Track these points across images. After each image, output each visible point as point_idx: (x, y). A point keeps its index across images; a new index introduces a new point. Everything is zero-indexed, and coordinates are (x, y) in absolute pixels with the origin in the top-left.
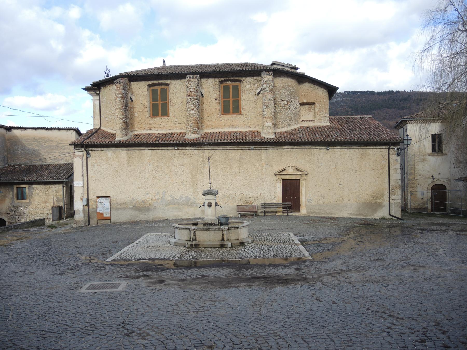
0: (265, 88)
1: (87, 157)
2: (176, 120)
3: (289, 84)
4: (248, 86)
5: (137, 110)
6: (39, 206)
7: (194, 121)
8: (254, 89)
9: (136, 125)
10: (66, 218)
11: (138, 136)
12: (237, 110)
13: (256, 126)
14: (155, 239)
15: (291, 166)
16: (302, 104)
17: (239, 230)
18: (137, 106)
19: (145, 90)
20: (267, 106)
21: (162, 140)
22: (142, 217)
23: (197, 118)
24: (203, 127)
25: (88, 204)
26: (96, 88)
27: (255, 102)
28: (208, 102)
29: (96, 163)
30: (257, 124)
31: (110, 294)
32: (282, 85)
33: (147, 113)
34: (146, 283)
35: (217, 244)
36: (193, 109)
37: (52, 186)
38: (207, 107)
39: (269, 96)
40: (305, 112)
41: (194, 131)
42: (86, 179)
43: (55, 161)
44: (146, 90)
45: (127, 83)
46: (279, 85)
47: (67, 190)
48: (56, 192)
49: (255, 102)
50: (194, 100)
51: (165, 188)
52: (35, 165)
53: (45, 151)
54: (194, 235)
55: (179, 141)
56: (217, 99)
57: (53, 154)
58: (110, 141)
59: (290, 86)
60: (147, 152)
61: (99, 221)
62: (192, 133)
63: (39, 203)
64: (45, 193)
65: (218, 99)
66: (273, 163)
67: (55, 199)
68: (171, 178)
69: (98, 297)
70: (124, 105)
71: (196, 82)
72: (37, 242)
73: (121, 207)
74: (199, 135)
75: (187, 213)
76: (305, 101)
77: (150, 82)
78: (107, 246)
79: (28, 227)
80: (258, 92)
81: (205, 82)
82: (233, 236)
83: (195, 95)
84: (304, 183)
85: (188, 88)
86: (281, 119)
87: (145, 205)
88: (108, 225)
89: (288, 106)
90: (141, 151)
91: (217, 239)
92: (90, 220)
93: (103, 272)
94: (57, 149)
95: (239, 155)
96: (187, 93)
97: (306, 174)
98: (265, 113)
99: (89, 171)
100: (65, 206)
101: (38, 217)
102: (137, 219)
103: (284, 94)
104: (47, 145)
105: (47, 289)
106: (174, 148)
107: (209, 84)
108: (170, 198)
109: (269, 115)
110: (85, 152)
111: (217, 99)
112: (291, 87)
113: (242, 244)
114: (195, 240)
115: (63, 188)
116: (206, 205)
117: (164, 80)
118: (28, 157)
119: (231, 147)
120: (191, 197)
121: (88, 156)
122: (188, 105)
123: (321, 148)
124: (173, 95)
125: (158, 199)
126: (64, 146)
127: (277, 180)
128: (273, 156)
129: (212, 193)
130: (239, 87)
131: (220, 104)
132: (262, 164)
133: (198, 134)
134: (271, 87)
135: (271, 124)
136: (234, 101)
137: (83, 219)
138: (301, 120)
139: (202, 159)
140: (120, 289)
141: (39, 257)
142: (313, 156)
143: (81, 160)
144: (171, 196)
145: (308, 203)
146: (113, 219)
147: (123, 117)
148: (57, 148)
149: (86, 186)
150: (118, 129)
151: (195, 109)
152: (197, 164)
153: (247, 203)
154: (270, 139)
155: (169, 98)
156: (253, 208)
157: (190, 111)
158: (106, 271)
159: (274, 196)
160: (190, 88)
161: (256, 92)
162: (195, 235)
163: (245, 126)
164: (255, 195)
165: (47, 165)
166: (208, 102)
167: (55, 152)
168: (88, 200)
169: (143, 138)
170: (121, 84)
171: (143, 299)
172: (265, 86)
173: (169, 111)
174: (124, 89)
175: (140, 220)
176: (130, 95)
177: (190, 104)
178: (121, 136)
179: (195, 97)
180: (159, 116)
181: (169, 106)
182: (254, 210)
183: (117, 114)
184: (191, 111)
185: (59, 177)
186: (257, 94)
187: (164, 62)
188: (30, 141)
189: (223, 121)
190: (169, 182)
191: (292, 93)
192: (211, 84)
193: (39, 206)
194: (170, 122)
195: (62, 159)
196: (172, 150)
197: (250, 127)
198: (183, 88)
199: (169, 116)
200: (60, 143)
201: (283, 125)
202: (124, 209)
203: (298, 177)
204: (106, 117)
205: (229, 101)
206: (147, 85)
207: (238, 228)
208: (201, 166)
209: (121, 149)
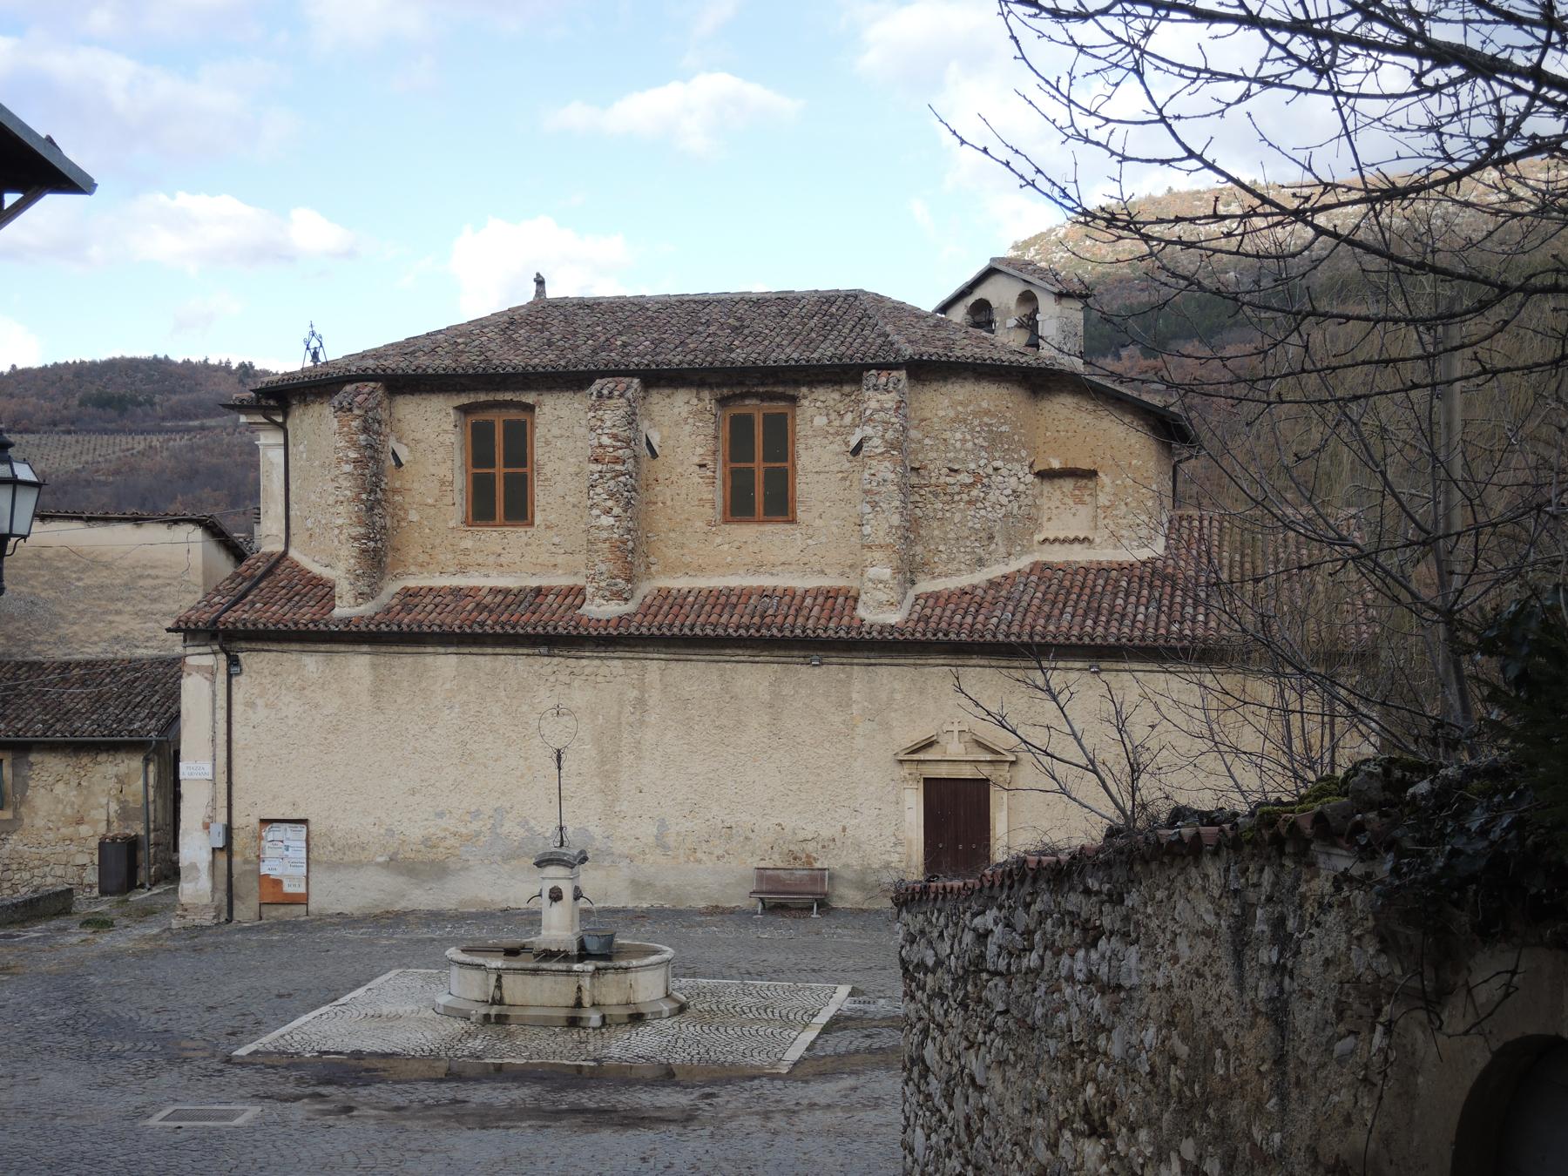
0: (870, 438)
1: (230, 676)
2: (556, 540)
3: (985, 405)
4: (820, 421)
6: (51, 836)
7: (612, 552)
9: (414, 552)
10: (154, 884)
11: (417, 600)
12: (780, 505)
13: (847, 570)
14: (405, 991)
15: (956, 728)
16: (1046, 475)
17: (631, 976)
18: (416, 485)
20: (874, 505)
21: (496, 623)
22: (421, 898)
23: (624, 543)
24: (653, 568)
25: (228, 847)
26: (272, 403)
27: (844, 479)
28: (674, 478)
29: (261, 696)
30: (849, 562)
31: (211, 1130)
32: (952, 414)
34: (309, 1111)
36: (608, 511)
37: (102, 757)
38: (668, 493)
39: (882, 468)
40: (1058, 504)
41: (611, 591)
42: (225, 754)
43: (117, 647)
44: (451, 427)
45: (379, 404)
46: (941, 413)
47: (159, 774)
48: (121, 780)
49: (844, 479)
50: (613, 478)
51: (503, 793)
52: (39, 665)
53: (81, 606)
55: (555, 628)
56: (704, 466)
57: (110, 618)
58: (312, 621)
59: (987, 412)
60: (445, 664)
61: (264, 908)
62: (603, 597)
63: (51, 825)
64: (74, 783)
65: (711, 465)
66: (893, 714)
67: (114, 807)
68: (526, 759)
69: (182, 1135)
70: (364, 489)
71: (621, 412)
72: (45, 985)
74: (630, 603)
77: (464, 399)
78: (253, 1008)
79: (11, 923)
80: (854, 442)
81: (662, 403)
82: (611, 991)
83: (617, 460)
86: (945, 540)
87: (431, 856)
88: (296, 926)
89: (975, 493)
90: (420, 659)
91: (562, 1002)
92: (235, 902)
93: (213, 1082)
94: (127, 600)
95: (771, 684)
97: (1012, 763)
99: (235, 727)
100: (152, 835)
101: (45, 876)
102: (399, 906)
103: (958, 445)
104: (88, 582)
105: (70, 1118)
106: (537, 651)
107: (676, 410)
108: (521, 832)
109: (881, 537)
110: (223, 657)
111: (704, 466)
113: (637, 1018)
114: (500, 1002)
115: (146, 766)
116: (546, 894)
117: (514, 390)
118: (10, 628)
119: (740, 652)
120: (596, 831)
121: (234, 670)
123: (1070, 665)
124: (548, 449)
125: (478, 834)
126: (154, 588)
127: (905, 780)
128: (893, 691)
130: (789, 421)
131: (719, 483)
133: (626, 600)
134: (890, 435)
135: (889, 571)
136: (769, 473)
137: (207, 900)
138: (1039, 537)
139: (635, 693)
140: (238, 1121)
141: (50, 1038)
143: (208, 683)
144: (524, 823)
146: (318, 902)
147: (362, 531)
148: (126, 594)
149: (223, 778)
150: (343, 575)
151: (617, 511)
152: (620, 713)
153: (795, 859)
156: (814, 880)
157: (598, 516)
158: (223, 1080)
160: (599, 431)
161: (847, 444)
162: (499, 986)
164: (826, 833)
165: (88, 663)
166: (674, 478)
167: (119, 612)
168: (229, 830)
169: (431, 607)
170: (356, 412)
171: (278, 1144)
172: (869, 431)
174: (365, 430)
176: (392, 443)
177: (599, 490)
178: (352, 601)
179: (618, 467)
180: (497, 521)
182: (819, 890)
183: (339, 522)
185: (131, 722)
187: (540, 282)
188: (19, 564)
189: (726, 547)
190: (519, 774)
191: (995, 440)
192: (686, 408)
193: (51, 836)
194: (534, 547)
195: (148, 639)
196: (530, 660)
197: (822, 572)
199: (532, 524)
200: (140, 577)
201: (953, 566)
202: (358, 865)
203: (985, 771)
204: (306, 513)
205: (751, 472)
206: (456, 408)
207: (627, 969)
209: (351, 648)
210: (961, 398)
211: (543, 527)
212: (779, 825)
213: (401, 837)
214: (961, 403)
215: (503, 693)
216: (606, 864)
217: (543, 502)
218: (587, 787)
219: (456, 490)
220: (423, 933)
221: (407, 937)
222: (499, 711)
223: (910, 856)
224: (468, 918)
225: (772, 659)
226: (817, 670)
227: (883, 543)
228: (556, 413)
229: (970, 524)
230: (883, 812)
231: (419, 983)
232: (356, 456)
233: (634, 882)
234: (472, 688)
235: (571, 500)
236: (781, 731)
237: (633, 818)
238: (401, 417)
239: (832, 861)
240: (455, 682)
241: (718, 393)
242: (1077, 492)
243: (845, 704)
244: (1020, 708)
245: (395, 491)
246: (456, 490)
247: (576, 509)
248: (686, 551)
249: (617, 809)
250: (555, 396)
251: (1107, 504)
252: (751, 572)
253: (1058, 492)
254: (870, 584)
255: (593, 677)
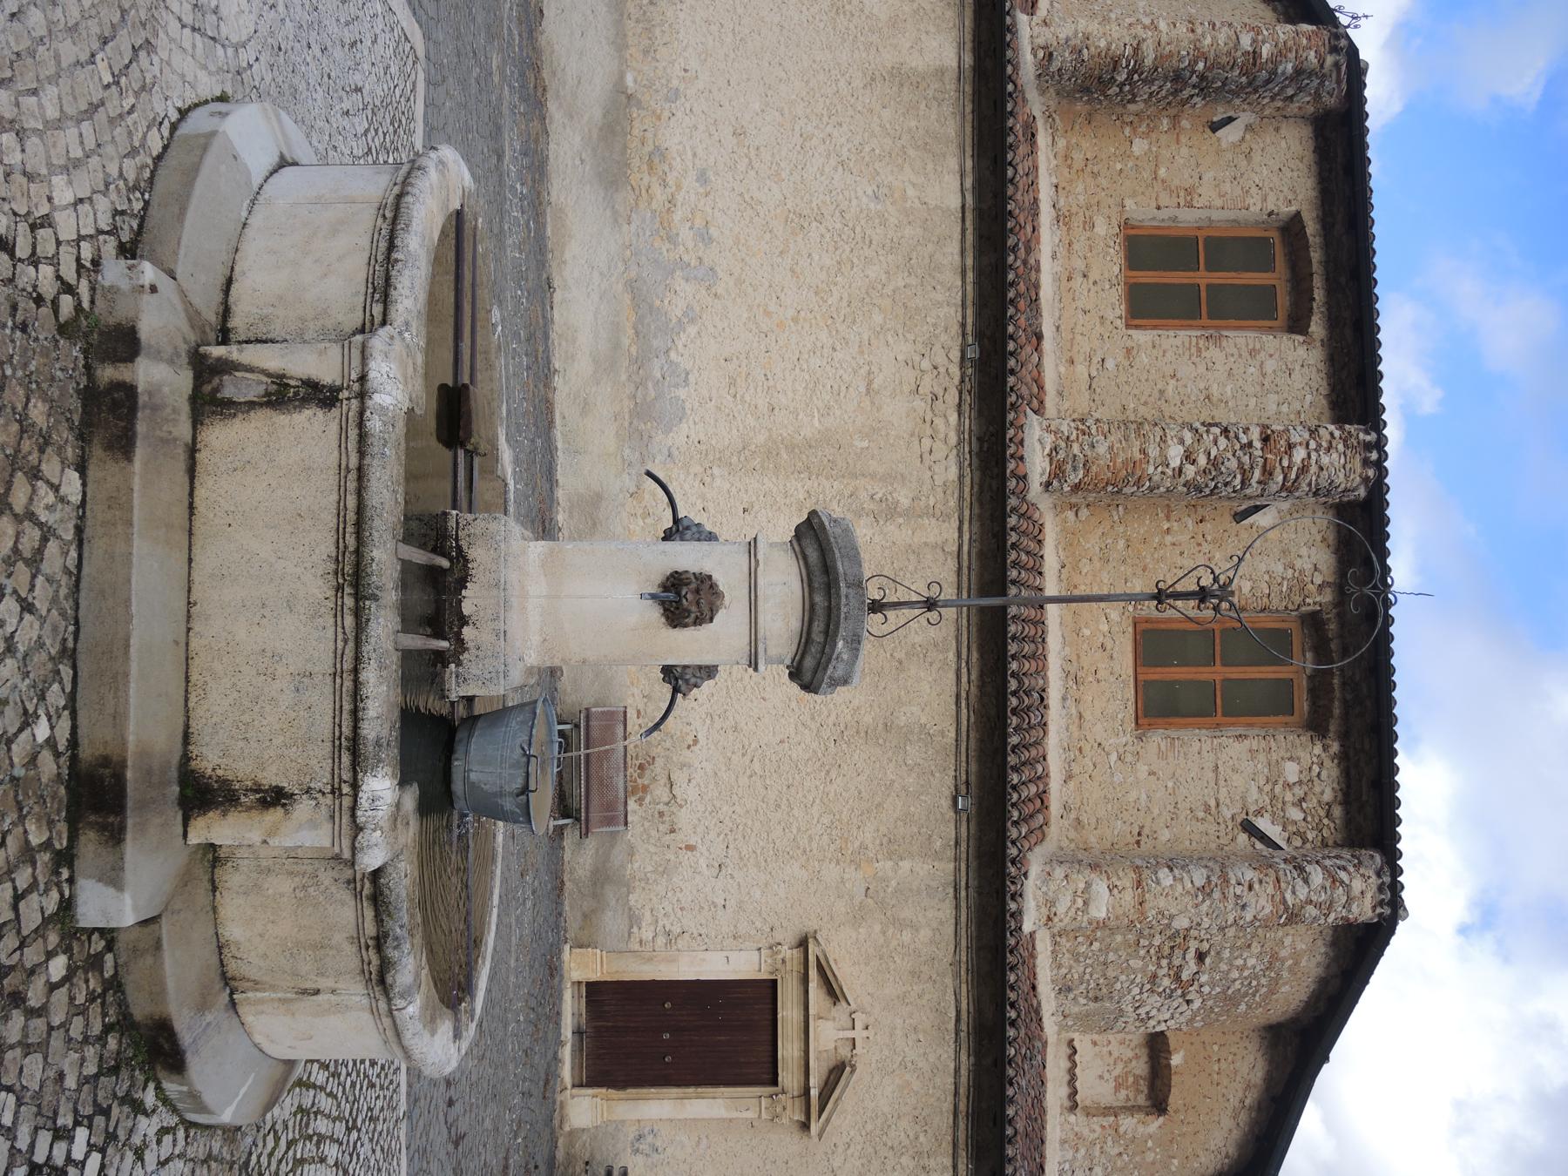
0: (1306, 881)
2: (1110, 364)
4: (1291, 771)
5: (1166, 154)
8: (1275, 807)
9: (1086, 146)
13: (1073, 815)
15: (859, 1034)
16: (1157, 1046)
17: (356, 993)
18: (1184, 151)
19: (1271, 198)
20: (1205, 891)
24: (1070, 515)
27: (1207, 809)
28: (1206, 547)
30: (1084, 818)
32: (1283, 953)
33: (1144, 211)
35: (118, 718)
36: (1189, 457)
39: (1262, 902)
40: (1116, 1054)
44: (1271, 207)
46: (1288, 941)
49: (1207, 809)
51: (739, 282)
54: (280, 380)
62: (1055, 449)
66: (877, 928)
68: (795, 320)
71: (1340, 479)
73: (631, 24)
75: (585, 408)
76: (1176, 1060)
77: (1311, 227)
80: (1263, 824)
81: (1314, 531)
83: (1268, 472)
84: (751, 1115)
85: (1306, 435)
87: (636, 162)
89: (1166, 982)
90: (953, 148)
96: (1277, 427)
98: (1166, 877)
103: (1240, 962)
106: (970, 340)
107: (1304, 551)
108: (677, 311)
112: (1265, 998)
116: (687, 557)
119: (973, 677)
122: (1216, 430)
124: (1245, 354)
125: (672, 239)
129: (830, 634)
130: (1281, 718)
132: (869, 861)
133: (1048, 484)
135: (1102, 914)
139: (905, 502)
142: (912, 1164)
144: (690, 317)
145: (632, 1132)
147: (1148, 62)
151: (1190, 471)
152: (873, 476)
153: (641, 767)
154: (1018, 915)
155: (1227, 328)
156: (610, 807)
157: (1182, 442)
159: (677, 930)
161: (1259, 813)
163: (1074, 750)
164: (684, 818)
166: (1206, 547)
173: (1155, 327)
175: (552, 128)
176: (1245, 118)
177: (1223, 442)
178: (1041, 41)
179: (1257, 474)
181: (1182, 327)
183: (1163, 25)
184: (1181, 449)
186: (1251, 818)
189: (1105, 628)
190: (772, 307)
191: (1230, 1001)
192: (1308, 567)
197: (1069, 777)
198: (1285, 408)
199: (1128, 326)
201: (1066, 960)
203: (789, 1077)
208: (863, 496)
210: (1303, 963)
211: (1129, 344)
212: (696, 742)
213: (666, 114)
214: (1296, 963)
215: (901, 283)
216: (627, 451)
217: (1166, 344)
218: (751, 421)
219: (1177, 212)
220: (512, 142)
221: (505, 110)
222: (872, 275)
223: (650, 960)
224: (536, 222)
225: (964, 728)
226: (946, 803)
227: (1146, 906)
228: (1298, 367)
229: (1123, 978)
230: (720, 912)
231: (375, 89)
232: (1264, 55)
233: (596, 499)
234: (908, 231)
235: (1170, 389)
236: (848, 743)
237: (703, 497)
238: (1283, 132)
239: (639, 829)
240: (917, 204)
241: (1330, 615)
242: (1131, 1080)
243: (892, 847)
244: (892, 1134)
245: (1175, 119)
246: (1177, 212)
247: (1157, 395)
248: (1098, 565)
249: (716, 471)
250: (1321, 366)
251: (1122, 1130)
252: (1068, 667)
253: (1130, 1054)
254: (1082, 886)
255: (929, 432)
